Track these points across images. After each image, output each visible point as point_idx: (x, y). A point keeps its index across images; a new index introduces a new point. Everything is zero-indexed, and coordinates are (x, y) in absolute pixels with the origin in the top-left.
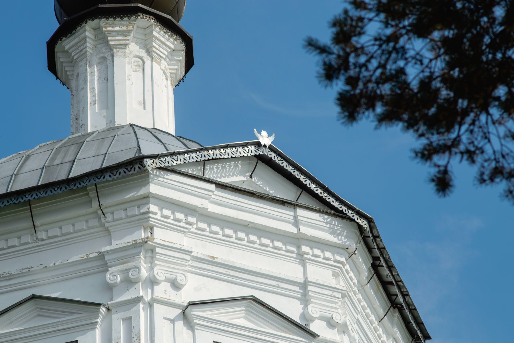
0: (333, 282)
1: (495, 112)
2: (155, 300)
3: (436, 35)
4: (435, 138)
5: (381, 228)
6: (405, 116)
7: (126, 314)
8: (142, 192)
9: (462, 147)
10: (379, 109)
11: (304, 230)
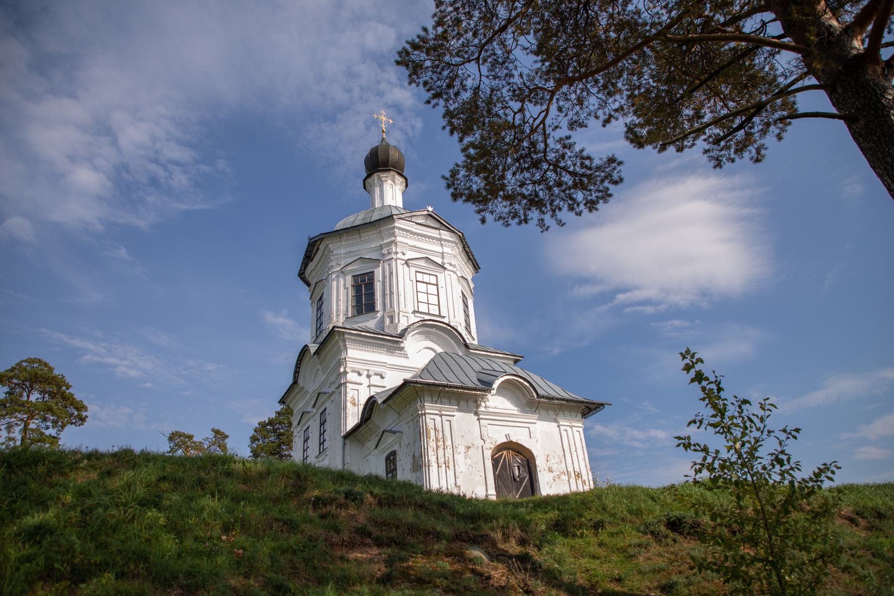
0: (451, 252)
1: (500, 200)
2: (397, 258)
3: (481, 175)
4: (481, 207)
5: (466, 236)
6: (472, 200)
7: (388, 263)
8: (393, 226)
9: (489, 210)
10: (464, 198)
11: (442, 237)
